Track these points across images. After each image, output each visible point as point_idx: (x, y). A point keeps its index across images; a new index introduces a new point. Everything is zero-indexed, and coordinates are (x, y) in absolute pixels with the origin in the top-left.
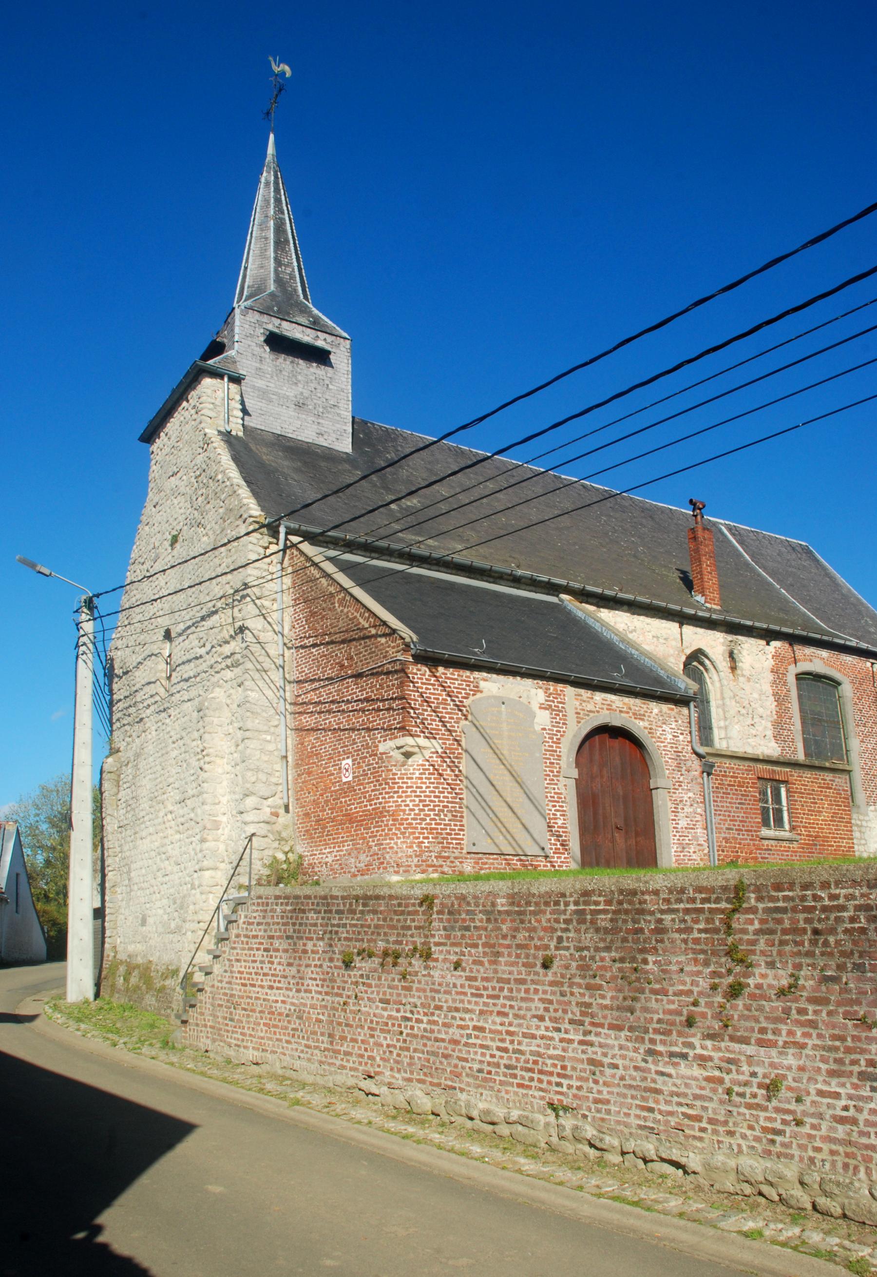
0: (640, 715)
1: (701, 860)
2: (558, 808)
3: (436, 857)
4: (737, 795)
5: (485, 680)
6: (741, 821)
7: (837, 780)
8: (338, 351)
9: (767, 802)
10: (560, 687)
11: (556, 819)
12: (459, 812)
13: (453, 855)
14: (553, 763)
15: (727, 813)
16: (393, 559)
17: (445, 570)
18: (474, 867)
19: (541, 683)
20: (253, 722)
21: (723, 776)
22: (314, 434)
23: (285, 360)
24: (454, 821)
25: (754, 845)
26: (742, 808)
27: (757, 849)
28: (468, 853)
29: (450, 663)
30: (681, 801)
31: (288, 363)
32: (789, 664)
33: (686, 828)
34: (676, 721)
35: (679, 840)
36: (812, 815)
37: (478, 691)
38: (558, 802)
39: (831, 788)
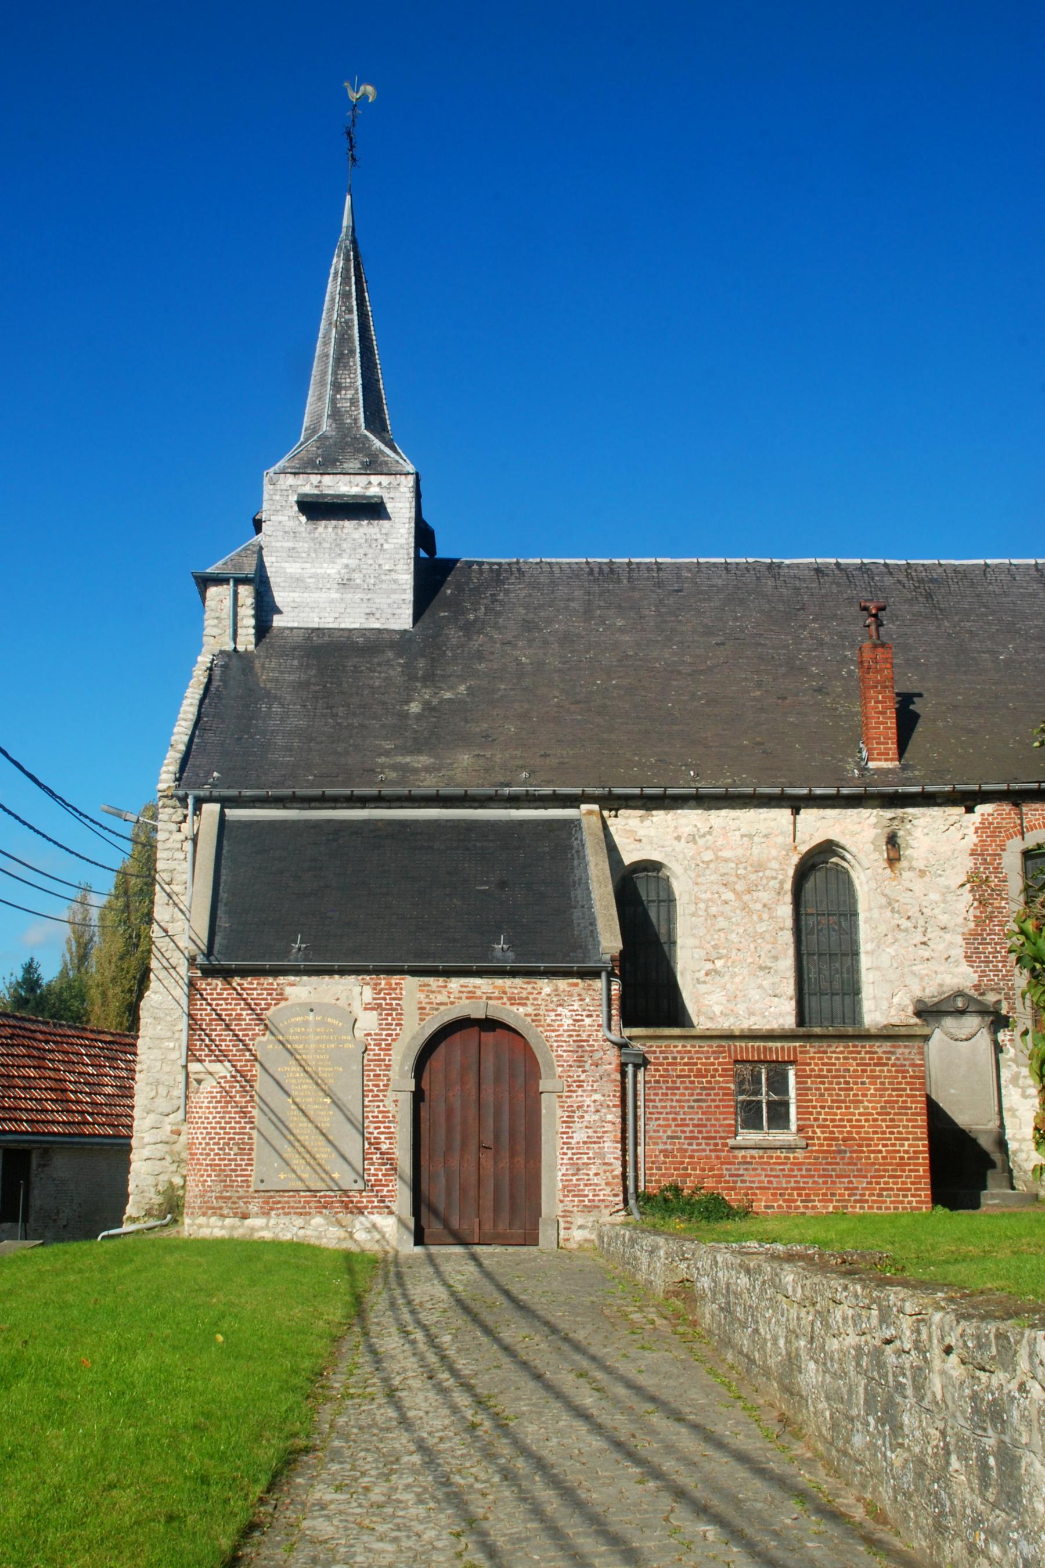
0: (521, 998)
1: (607, 1184)
2: (382, 1130)
3: (217, 1198)
7: (900, 1051)
8: (397, 494)
9: (758, 1092)
10: (395, 979)
11: (379, 1143)
12: (247, 1144)
13: (237, 1195)
14: (379, 1075)
15: (670, 1116)
16: (339, 805)
17: (410, 805)
18: (262, 1208)
19: (368, 978)
20: (155, 1029)
21: (669, 1064)
22: (363, 615)
23: (326, 527)
24: (241, 1154)
26: (700, 1107)
27: (722, 1163)
28: (256, 1191)
29: (244, 973)
30: (579, 1107)
31: (330, 530)
32: (1010, 837)
33: (585, 1143)
37: (282, 999)
39: (886, 1065)
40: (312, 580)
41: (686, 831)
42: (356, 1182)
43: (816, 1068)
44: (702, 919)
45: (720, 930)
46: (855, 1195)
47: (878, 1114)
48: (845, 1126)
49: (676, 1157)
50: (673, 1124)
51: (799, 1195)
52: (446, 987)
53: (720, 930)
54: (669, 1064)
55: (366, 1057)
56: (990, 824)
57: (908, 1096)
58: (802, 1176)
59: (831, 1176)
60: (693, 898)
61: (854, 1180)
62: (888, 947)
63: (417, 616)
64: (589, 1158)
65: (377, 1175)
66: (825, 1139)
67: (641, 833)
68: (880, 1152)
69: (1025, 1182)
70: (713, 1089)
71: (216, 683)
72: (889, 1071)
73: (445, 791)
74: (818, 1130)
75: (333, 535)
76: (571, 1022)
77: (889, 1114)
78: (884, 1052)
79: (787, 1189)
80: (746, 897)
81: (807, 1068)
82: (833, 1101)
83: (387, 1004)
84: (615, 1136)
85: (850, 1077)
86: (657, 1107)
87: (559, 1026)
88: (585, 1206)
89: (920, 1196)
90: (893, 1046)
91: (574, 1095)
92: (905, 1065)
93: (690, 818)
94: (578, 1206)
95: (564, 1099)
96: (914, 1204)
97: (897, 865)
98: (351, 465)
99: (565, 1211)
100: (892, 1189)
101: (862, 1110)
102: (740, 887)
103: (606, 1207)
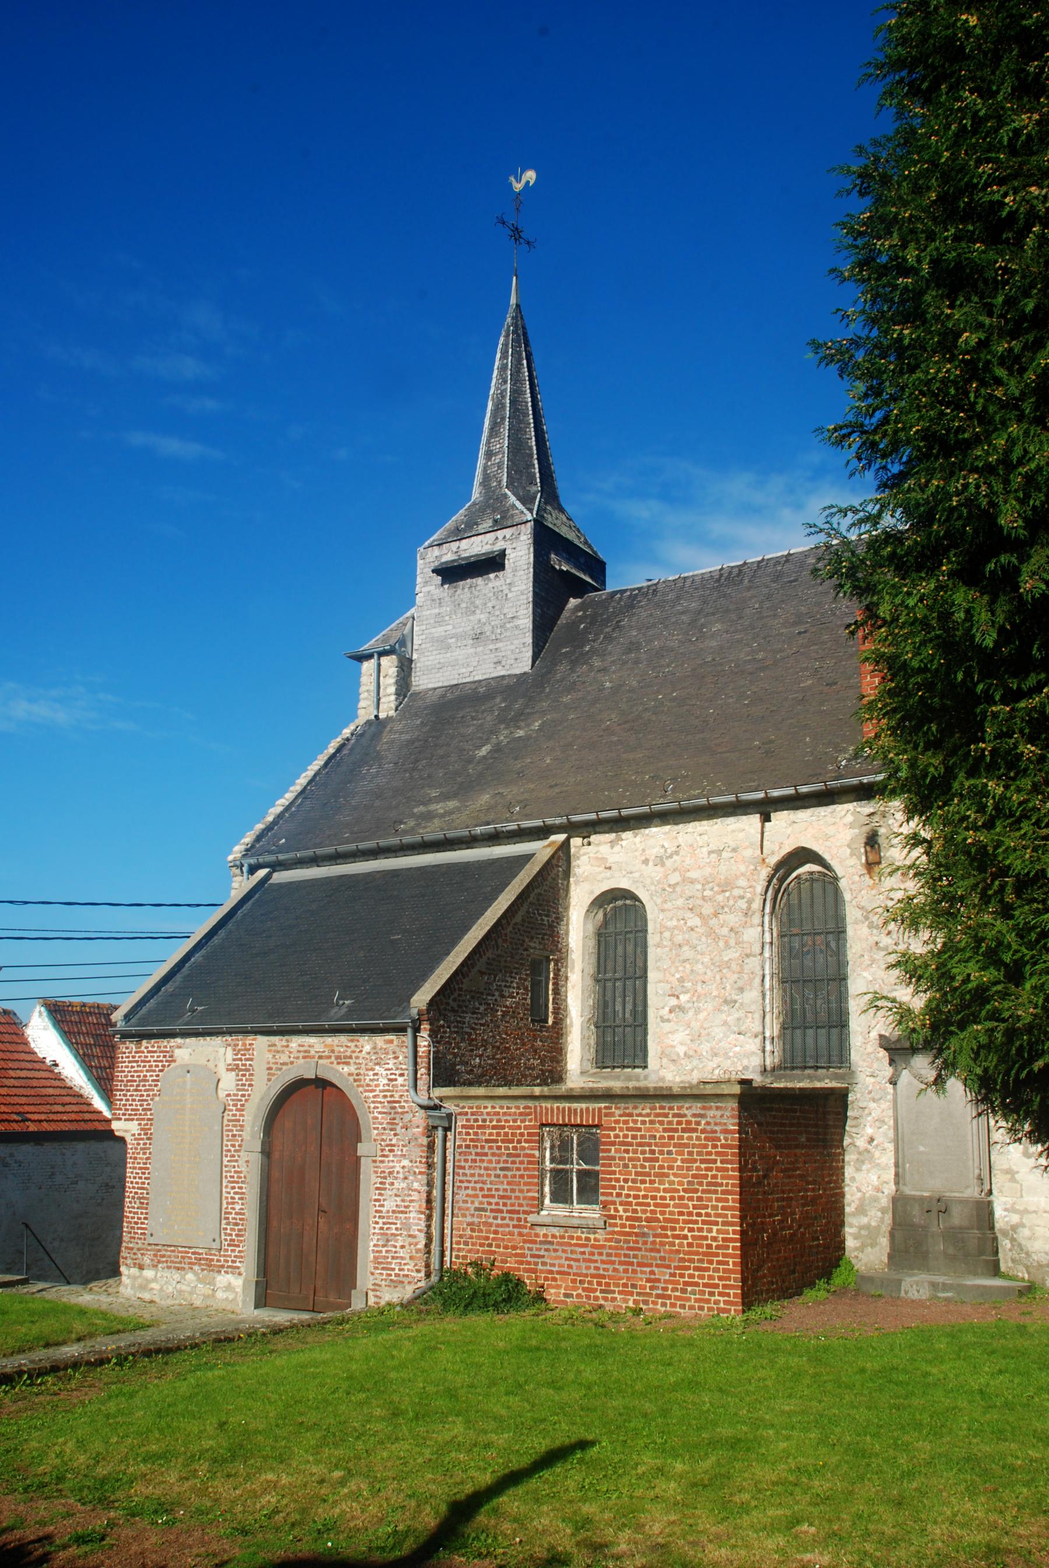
1: (411, 1258)
4: (500, 1155)
5: (179, 1047)
6: (501, 1197)
7: (711, 1113)
10: (249, 1039)
11: (233, 1203)
13: (137, 1246)
15: (478, 1186)
21: (479, 1127)
25: (520, 1234)
26: (505, 1176)
30: (390, 1173)
33: (394, 1212)
34: (396, 1058)
35: (381, 1228)
36: (643, 1182)
38: (238, 1182)
39: (695, 1130)
40: (453, 640)
41: (654, 852)
43: (621, 1134)
44: (667, 949)
45: (684, 961)
46: (657, 1288)
47: (684, 1190)
48: (648, 1205)
49: (481, 1231)
50: (481, 1194)
51: (599, 1284)
52: (288, 1046)
53: (684, 961)
54: (479, 1127)
55: (226, 1118)
57: (718, 1169)
58: (603, 1262)
59: (632, 1264)
60: (658, 926)
61: (656, 1270)
62: (864, 970)
63: (535, 657)
64: (397, 1229)
66: (628, 1218)
67: (611, 860)
68: (686, 1237)
69: (1027, 1268)
70: (518, 1156)
71: (345, 752)
72: (698, 1138)
73: (452, 834)
74: (620, 1208)
75: (468, 594)
76: (386, 1081)
77: (696, 1191)
78: (694, 1115)
79: (586, 1275)
80: (713, 922)
81: (612, 1134)
82: (637, 1174)
84: (420, 1206)
85: (656, 1145)
88: (391, 1280)
89: (728, 1295)
90: (704, 1108)
91: (386, 1159)
92: (715, 1132)
93: (658, 836)
94: (386, 1280)
95: (378, 1164)
96: (722, 1305)
97: (876, 869)
98: (485, 525)
99: (374, 1284)
100: (697, 1284)
101: (667, 1186)
102: (708, 909)
103: (409, 1283)
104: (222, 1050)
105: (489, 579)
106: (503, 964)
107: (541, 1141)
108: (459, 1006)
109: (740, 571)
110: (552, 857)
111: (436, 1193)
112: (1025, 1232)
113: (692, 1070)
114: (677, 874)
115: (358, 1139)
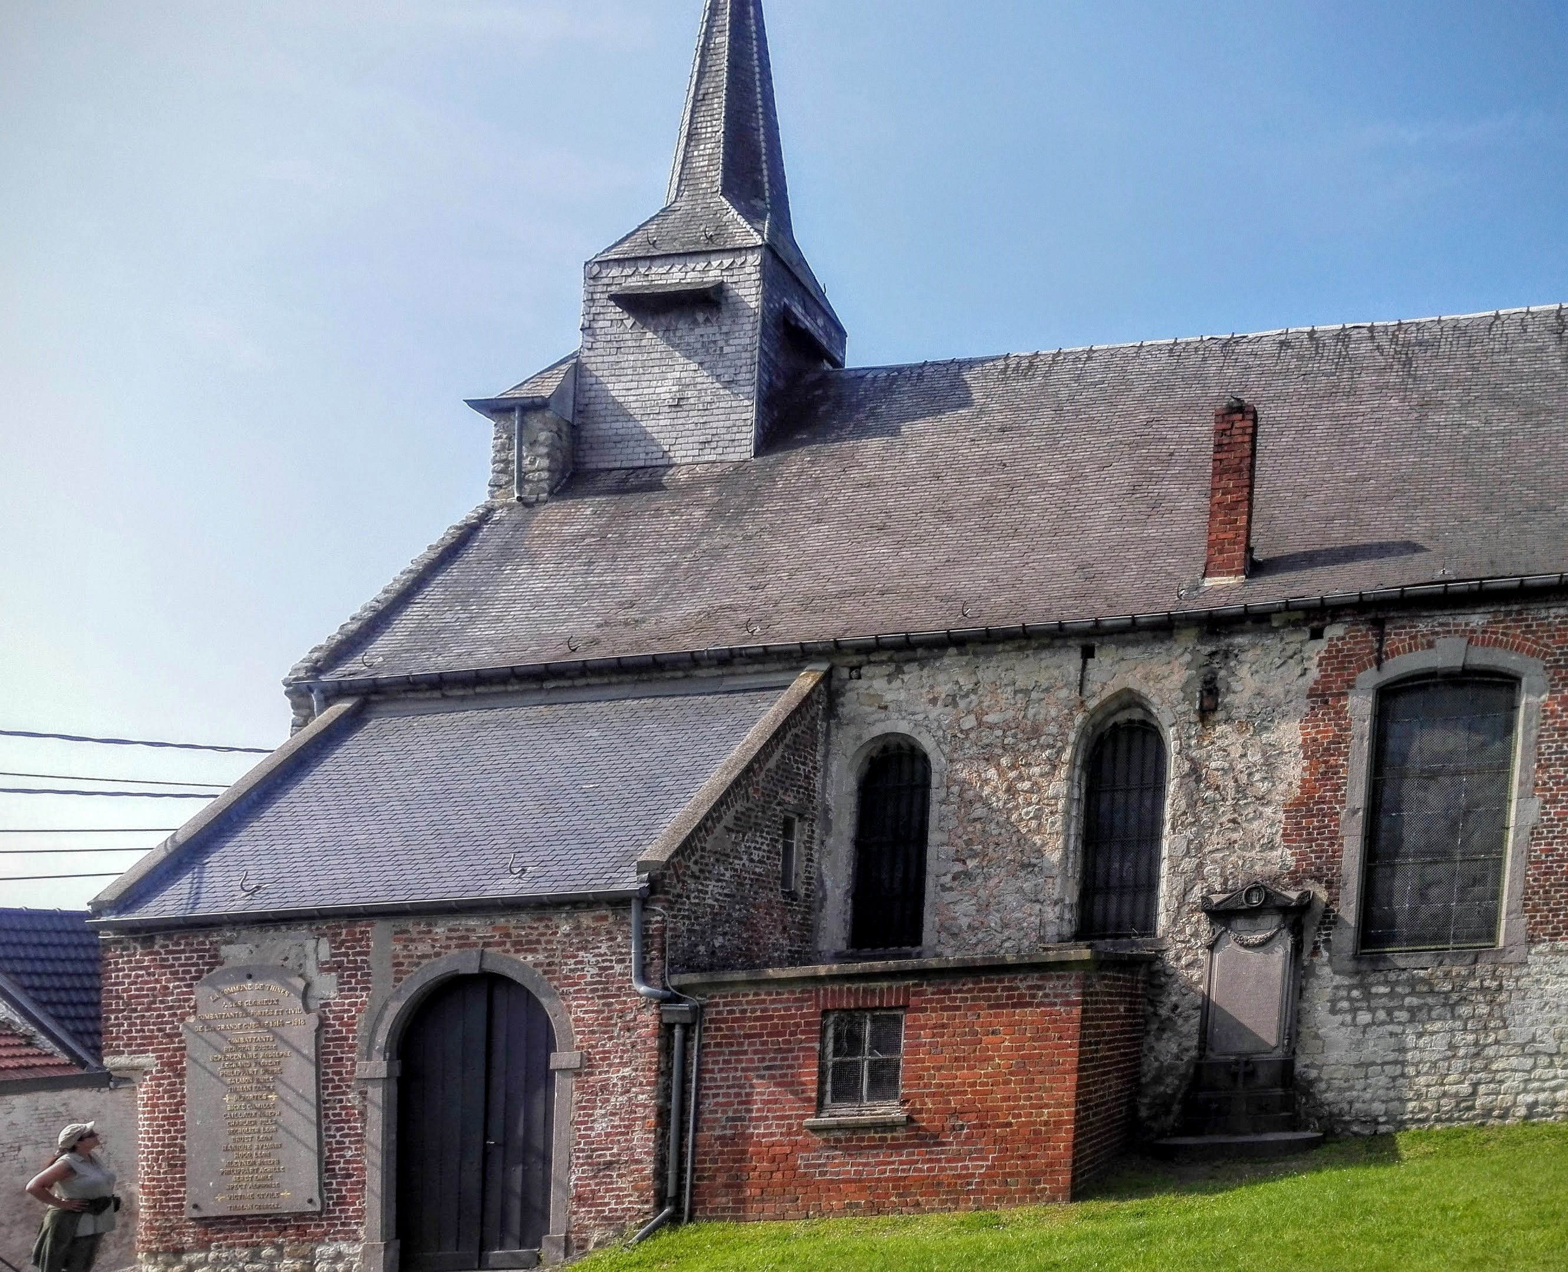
0: (530, 942)
11: (342, 1149)
15: (732, 1091)
21: (734, 1020)
32: (1362, 668)
33: (608, 1135)
39: (1030, 1004)
42: (310, 1201)
48: (965, 1092)
52: (430, 932)
53: (975, 820)
54: (734, 1020)
56: (1339, 651)
65: (340, 1191)
67: (889, 697)
76: (596, 971)
78: (1030, 988)
83: (349, 962)
86: (715, 1080)
87: (580, 977)
90: (1041, 978)
103: (631, 1218)
104: (311, 944)
105: (695, 322)
106: (753, 820)
107: (823, 1032)
108: (701, 871)
109: (1031, 364)
110: (813, 690)
111: (674, 1105)
112: (1323, 1086)
113: (976, 945)
114: (972, 717)
115: (550, 1046)
